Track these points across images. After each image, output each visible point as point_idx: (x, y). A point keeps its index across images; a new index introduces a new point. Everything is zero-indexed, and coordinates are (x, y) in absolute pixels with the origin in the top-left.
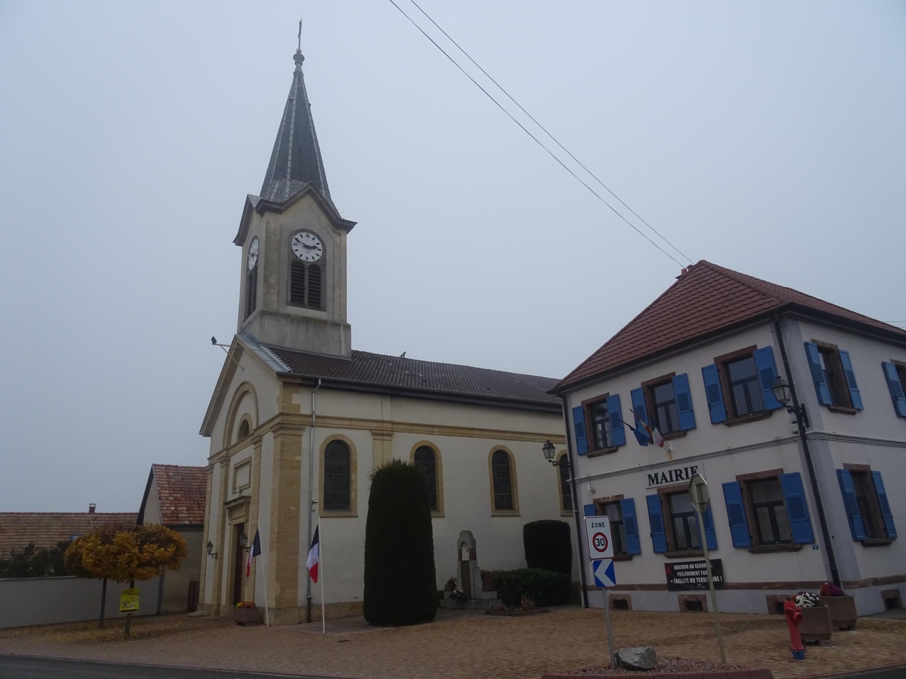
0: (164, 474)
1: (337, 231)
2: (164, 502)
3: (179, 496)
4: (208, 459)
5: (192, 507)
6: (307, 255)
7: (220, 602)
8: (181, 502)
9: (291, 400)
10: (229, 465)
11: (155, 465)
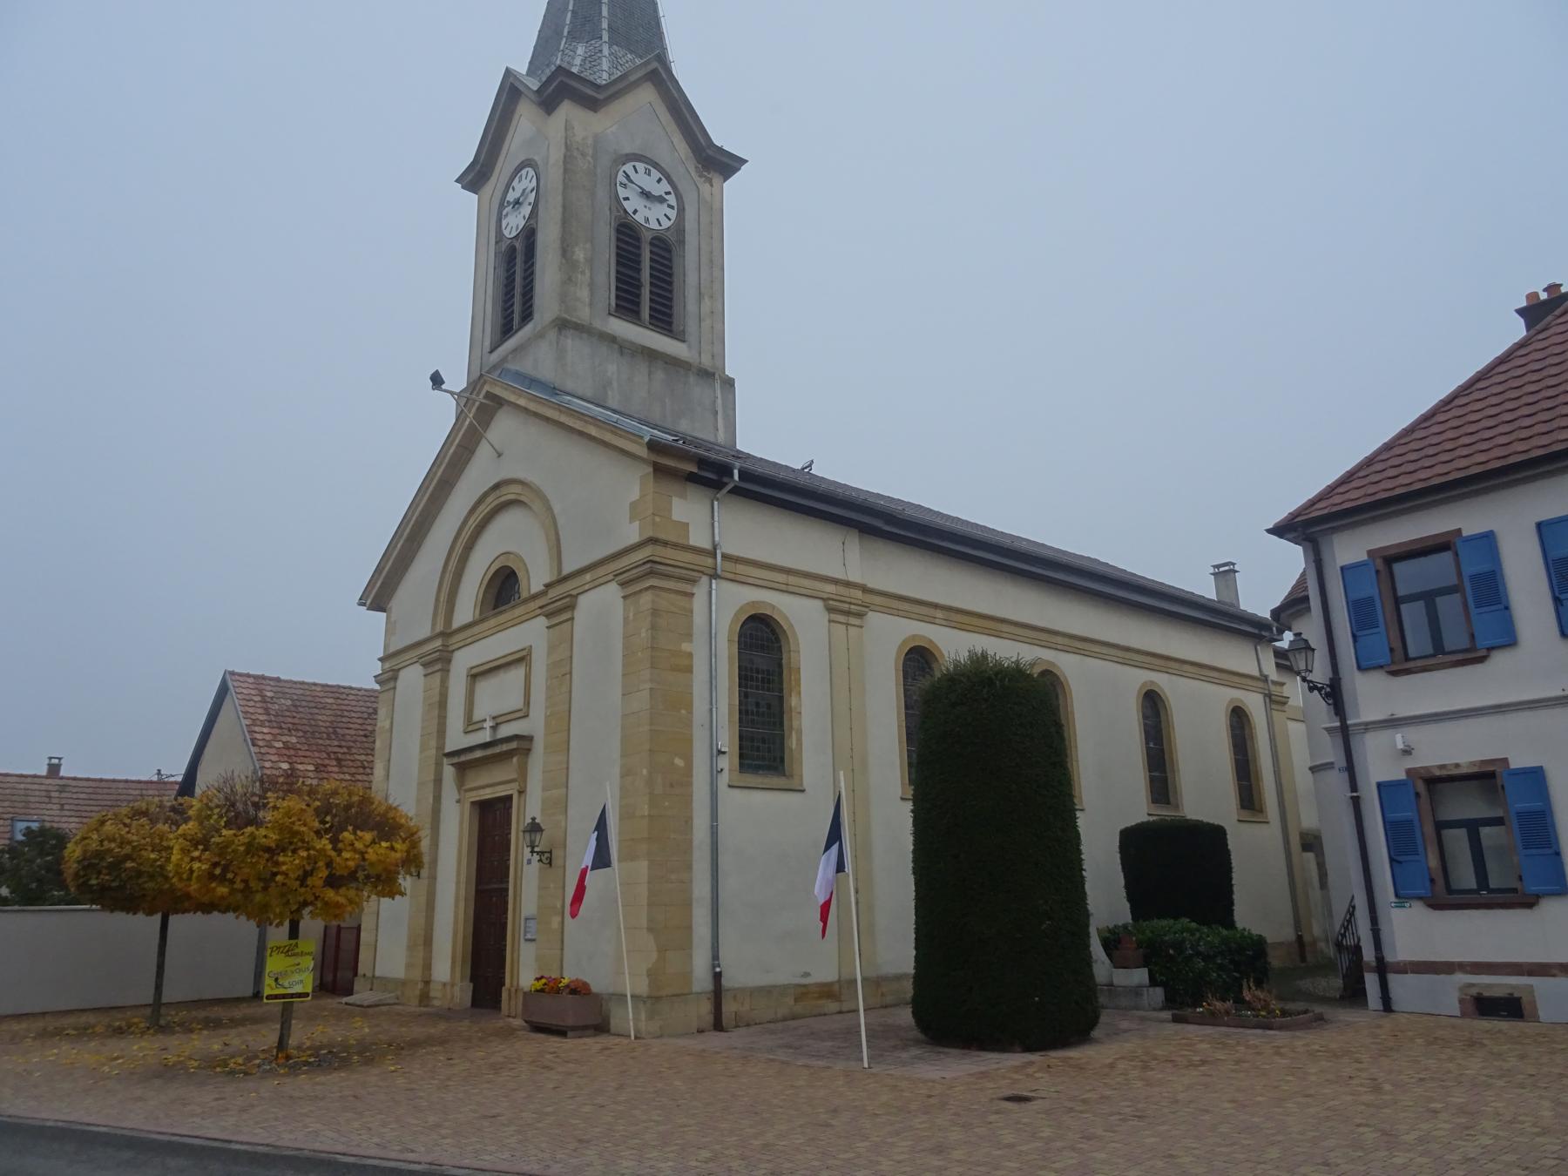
0: (253, 692)
1: (706, 173)
2: (263, 750)
3: (294, 740)
4: (380, 659)
5: (325, 766)
6: (647, 213)
7: (430, 975)
8: (300, 753)
9: (670, 511)
10: (448, 671)
11: (233, 673)
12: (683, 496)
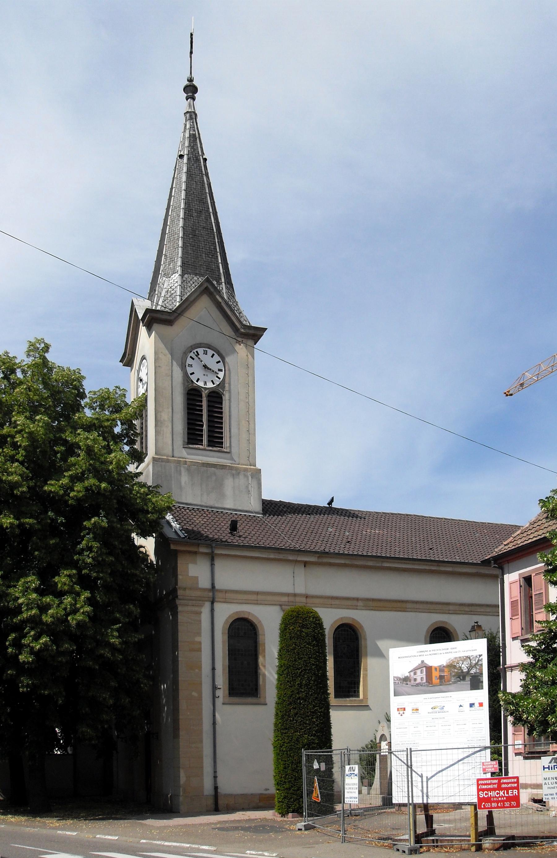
12: (195, 563)
